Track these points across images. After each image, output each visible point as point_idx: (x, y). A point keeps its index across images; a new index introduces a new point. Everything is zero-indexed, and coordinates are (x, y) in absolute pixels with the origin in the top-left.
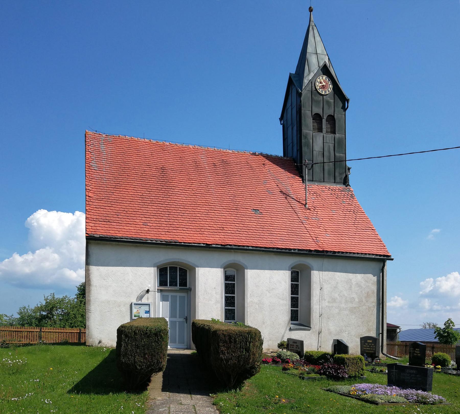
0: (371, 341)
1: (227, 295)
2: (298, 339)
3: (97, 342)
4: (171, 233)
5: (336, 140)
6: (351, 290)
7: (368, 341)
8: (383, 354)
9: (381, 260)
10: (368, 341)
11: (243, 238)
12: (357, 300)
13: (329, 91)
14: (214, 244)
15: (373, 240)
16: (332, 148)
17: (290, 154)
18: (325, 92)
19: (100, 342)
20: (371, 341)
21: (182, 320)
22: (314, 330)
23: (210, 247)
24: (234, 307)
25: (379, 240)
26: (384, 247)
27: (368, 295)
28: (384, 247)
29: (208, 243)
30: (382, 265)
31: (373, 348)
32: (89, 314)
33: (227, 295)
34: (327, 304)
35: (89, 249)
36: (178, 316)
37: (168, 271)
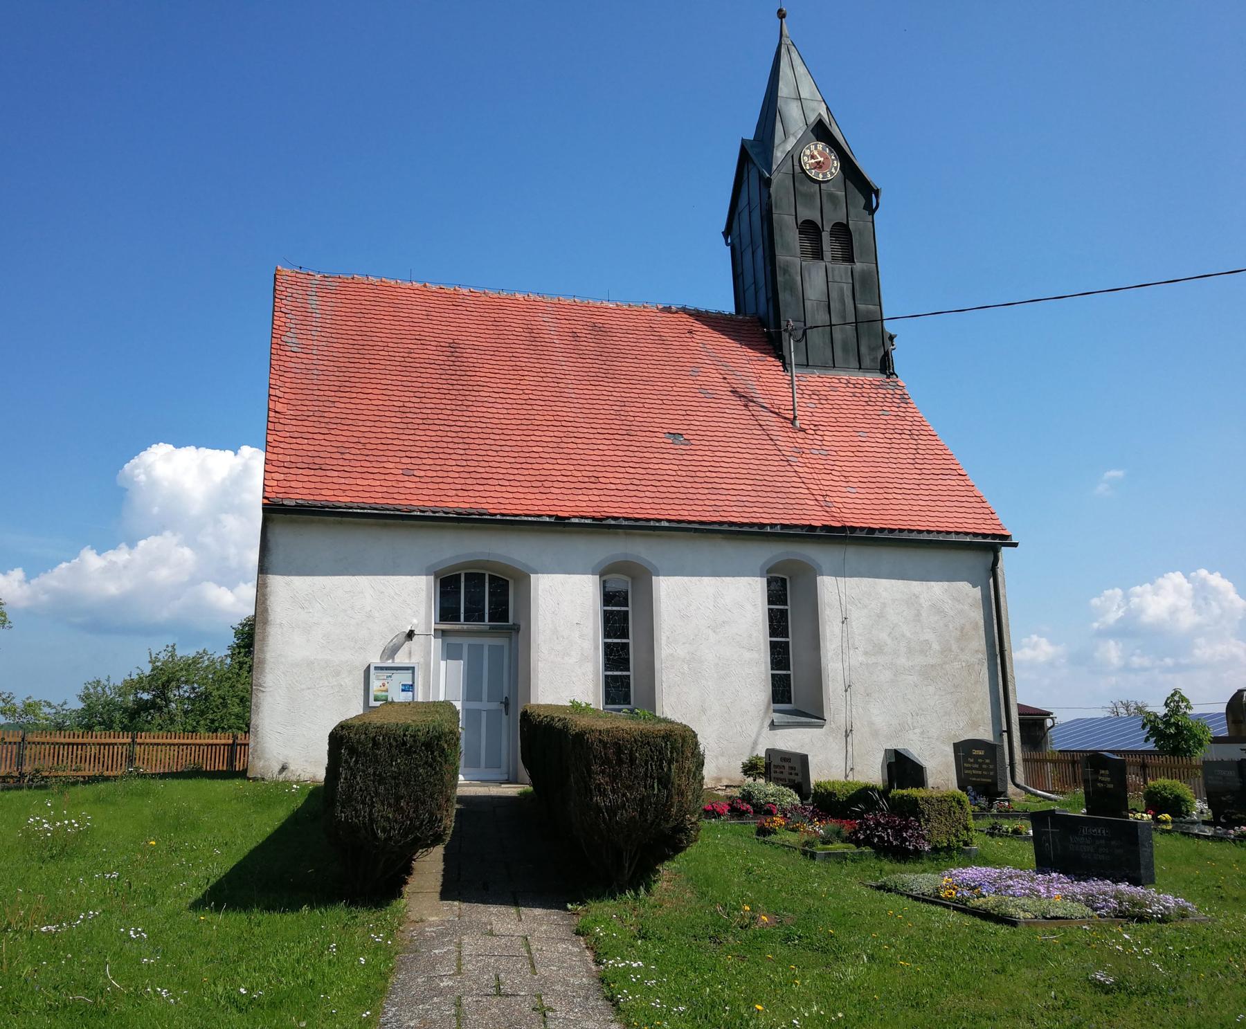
0: (981, 753)
3: (277, 768)
7: (975, 752)
10: (975, 752)
12: (936, 646)
20: (981, 753)
21: (494, 706)
22: (833, 726)
27: (963, 636)
31: (988, 770)
32: (260, 695)
36: (485, 696)
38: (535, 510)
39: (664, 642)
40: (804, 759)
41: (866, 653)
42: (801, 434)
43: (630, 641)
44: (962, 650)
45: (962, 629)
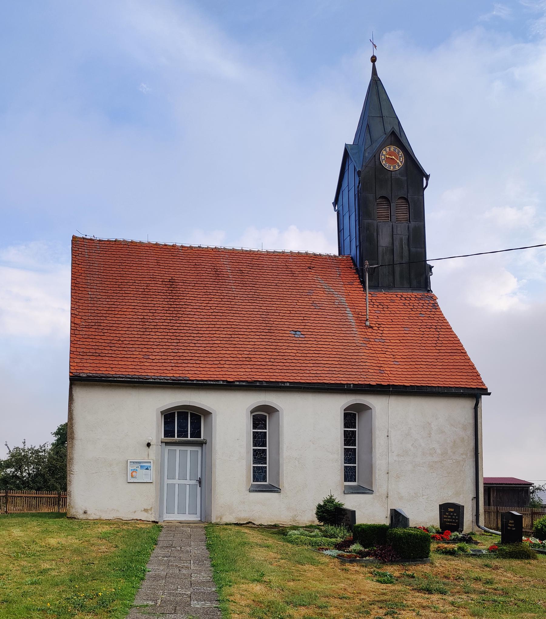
0: (452, 510)
3: (81, 512)
4: (180, 368)
5: (411, 230)
6: (430, 437)
7: (450, 510)
8: (479, 527)
9: (475, 393)
10: (450, 510)
11: (277, 371)
12: (439, 451)
13: (399, 166)
16: (405, 242)
17: (347, 252)
18: (394, 167)
19: (85, 513)
20: (452, 510)
23: (231, 386)
29: (228, 380)
36: (188, 478)
40: (440, 505)
41: (398, 455)
43: (267, 448)
44: (454, 453)
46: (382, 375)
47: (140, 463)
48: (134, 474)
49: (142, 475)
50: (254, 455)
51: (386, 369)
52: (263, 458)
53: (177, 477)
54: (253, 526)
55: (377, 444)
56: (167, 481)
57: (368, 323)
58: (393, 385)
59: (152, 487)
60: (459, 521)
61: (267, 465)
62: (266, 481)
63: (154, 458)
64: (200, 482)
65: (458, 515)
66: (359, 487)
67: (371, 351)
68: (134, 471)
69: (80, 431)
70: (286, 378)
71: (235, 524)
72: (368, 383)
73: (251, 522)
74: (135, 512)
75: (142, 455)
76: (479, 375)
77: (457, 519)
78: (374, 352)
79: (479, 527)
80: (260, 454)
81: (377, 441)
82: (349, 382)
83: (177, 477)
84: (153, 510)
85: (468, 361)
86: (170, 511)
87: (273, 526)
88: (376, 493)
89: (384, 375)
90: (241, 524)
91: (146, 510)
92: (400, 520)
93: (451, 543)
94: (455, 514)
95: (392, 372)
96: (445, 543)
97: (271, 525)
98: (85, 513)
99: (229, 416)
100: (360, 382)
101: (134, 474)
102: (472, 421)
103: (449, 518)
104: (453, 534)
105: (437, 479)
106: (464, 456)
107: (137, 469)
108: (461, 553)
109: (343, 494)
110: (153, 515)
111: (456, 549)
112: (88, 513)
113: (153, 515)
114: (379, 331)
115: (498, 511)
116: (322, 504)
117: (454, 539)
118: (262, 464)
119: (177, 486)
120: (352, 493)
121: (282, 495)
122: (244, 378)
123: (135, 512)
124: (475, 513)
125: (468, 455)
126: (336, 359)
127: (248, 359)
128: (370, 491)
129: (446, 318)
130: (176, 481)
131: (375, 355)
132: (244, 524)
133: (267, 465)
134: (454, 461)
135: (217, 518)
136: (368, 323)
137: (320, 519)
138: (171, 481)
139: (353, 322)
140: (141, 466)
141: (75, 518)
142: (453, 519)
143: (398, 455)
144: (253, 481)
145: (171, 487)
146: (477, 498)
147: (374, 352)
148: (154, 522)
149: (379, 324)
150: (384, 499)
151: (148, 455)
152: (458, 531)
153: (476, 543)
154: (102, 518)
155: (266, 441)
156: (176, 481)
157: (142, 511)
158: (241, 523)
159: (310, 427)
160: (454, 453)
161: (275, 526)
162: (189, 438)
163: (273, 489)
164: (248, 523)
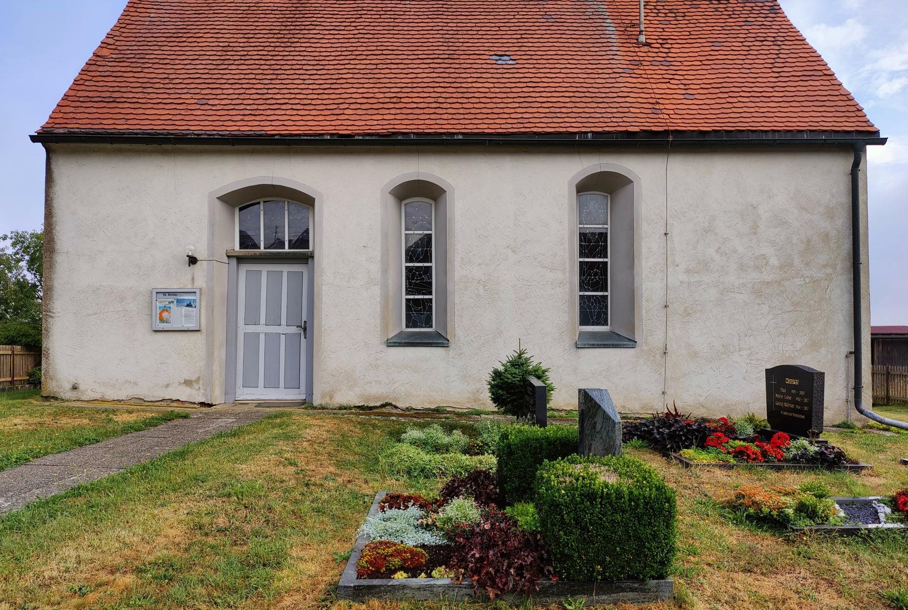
0: (795, 382)
1: (411, 264)
2: (809, 368)
3: (68, 386)
6: (755, 233)
7: (789, 381)
8: (861, 412)
9: (852, 140)
10: (789, 381)
12: (774, 261)
14: (359, 134)
15: (825, 98)
19: (75, 388)
20: (795, 382)
21: (293, 330)
22: (645, 348)
24: (431, 294)
25: (844, 98)
26: (859, 114)
27: (808, 248)
28: (859, 114)
30: (852, 161)
31: (802, 404)
32: (50, 320)
33: (411, 264)
34: (683, 277)
35: (53, 166)
36: (284, 321)
37: (262, 213)
38: (318, 130)
39: (457, 262)
40: (768, 372)
41: (688, 271)
42: (646, 49)
43: (433, 264)
44: (807, 264)
45: (809, 241)
46: (656, 116)
47: (175, 294)
48: (165, 315)
49: (179, 317)
50: (407, 278)
51: (667, 107)
52: (426, 283)
53: (263, 320)
54: (395, 411)
55: (644, 250)
56: (243, 329)
57: (642, 38)
58: (676, 130)
59: (197, 340)
60: (810, 410)
61: (433, 297)
62: (431, 326)
63: (204, 285)
64: (305, 329)
65: (810, 394)
66: (613, 334)
67: (640, 80)
68: (165, 309)
69: (65, 239)
70: (459, 126)
71: (359, 407)
72: (624, 129)
73: (390, 404)
74: (167, 386)
75: (182, 279)
76: (860, 110)
77: (806, 404)
78: (647, 81)
79: (861, 412)
80: (420, 275)
81: (643, 244)
82: (584, 130)
83: (263, 320)
84: (201, 382)
85: (838, 87)
86: (250, 383)
87: (434, 410)
88: (642, 346)
89: (661, 116)
90: (371, 408)
91: (188, 383)
92: (598, 426)
93: (788, 468)
94: (802, 393)
95: (677, 111)
96: (772, 467)
97: (429, 409)
98: (75, 388)
99: (351, 203)
100: (607, 129)
101: (165, 315)
102: (846, 200)
103: (788, 401)
104: (793, 443)
105: (771, 316)
106: (829, 271)
107: (171, 305)
108: (805, 524)
109: (385, 346)
110: (202, 391)
111: (790, 511)
112: (82, 387)
113: (202, 391)
114: (662, 50)
115: (888, 373)
116: (501, 368)
117: (794, 459)
118: (423, 294)
119: (262, 337)
120: (593, 346)
121: (452, 352)
122: (378, 129)
123: (167, 386)
124: (852, 384)
125: (839, 267)
126: (567, 94)
127: (394, 100)
128: (631, 343)
129: (795, 25)
130: (262, 329)
131: (648, 86)
132: (375, 407)
133: (433, 297)
134: (807, 280)
135: (323, 396)
136: (642, 38)
137: (496, 399)
138: (251, 329)
139: (615, 39)
140: (179, 301)
141: (56, 398)
142: (797, 403)
143: (688, 271)
144: (407, 326)
145: (251, 338)
146: (856, 353)
147: (647, 81)
148: (203, 404)
149: (663, 39)
150: (658, 357)
151: (193, 279)
152: (807, 436)
153: (857, 468)
154: (107, 397)
155: (431, 251)
156: (262, 329)
157: (180, 384)
158: (371, 405)
159: (512, 221)
160: (807, 264)
161: (437, 411)
162: (287, 249)
163: (439, 341)
164: (383, 406)
